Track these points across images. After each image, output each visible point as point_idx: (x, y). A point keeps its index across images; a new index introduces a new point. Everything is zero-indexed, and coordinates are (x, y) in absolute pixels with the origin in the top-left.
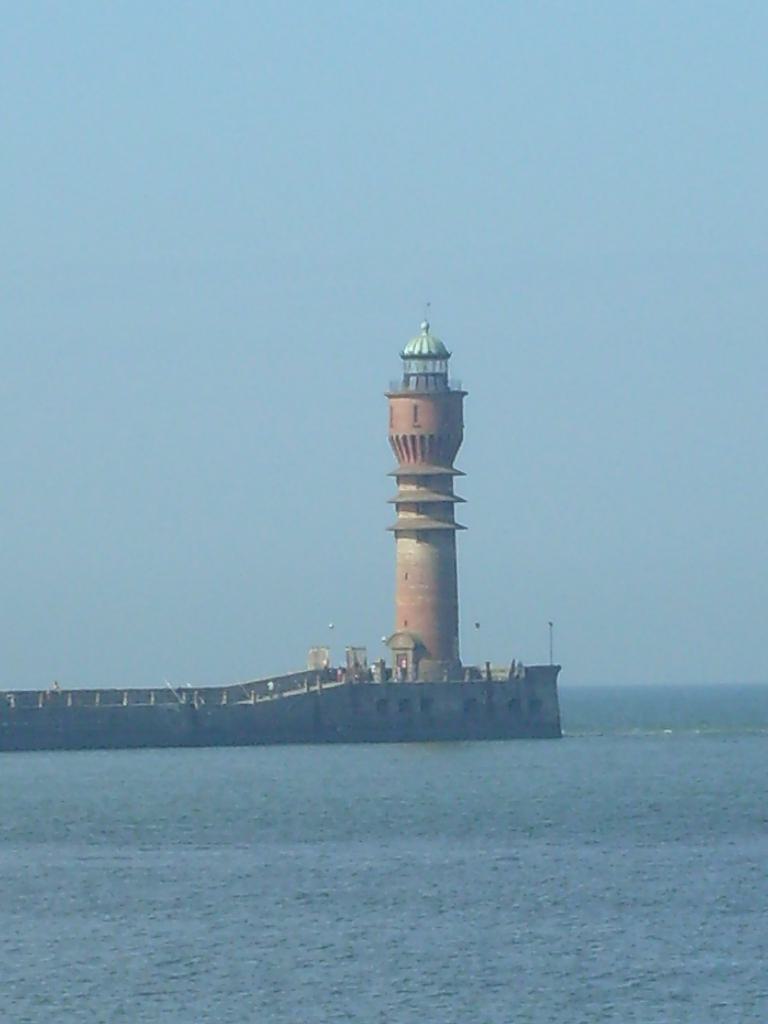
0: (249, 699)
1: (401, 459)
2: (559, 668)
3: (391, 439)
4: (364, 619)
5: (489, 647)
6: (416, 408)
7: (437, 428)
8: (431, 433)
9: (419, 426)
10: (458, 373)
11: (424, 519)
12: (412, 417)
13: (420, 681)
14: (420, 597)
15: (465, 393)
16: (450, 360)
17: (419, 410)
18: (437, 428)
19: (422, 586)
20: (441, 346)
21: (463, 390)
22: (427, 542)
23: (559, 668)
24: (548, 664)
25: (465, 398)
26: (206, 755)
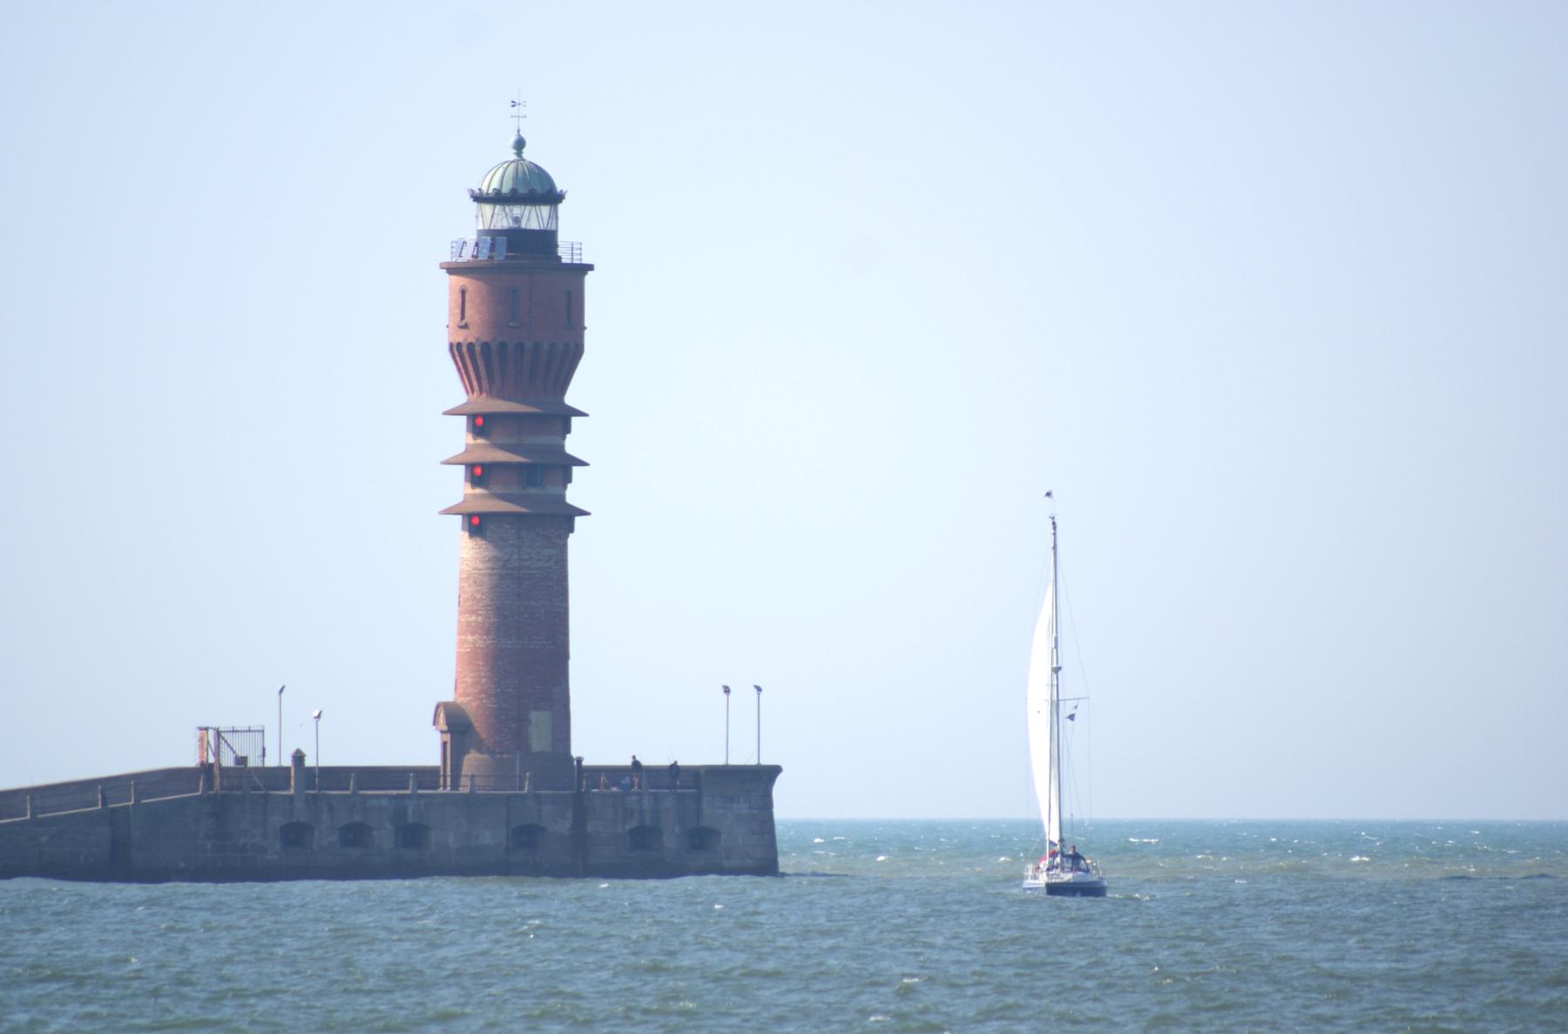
0: (436, 788)
1: (470, 389)
2: (775, 771)
3: (451, 346)
4: (380, 688)
5: (617, 718)
6: (463, 292)
7: (523, 317)
8: (485, 339)
9: (466, 327)
10: (576, 231)
11: (481, 496)
12: (458, 311)
13: (464, 790)
14: (470, 638)
15: (590, 267)
16: (560, 206)
17: (467, 297)
18: (523, 317)
19: (473, 618)
20: (540, 175)
21: (585, 261)
22: (484, 537)
23: (775, 771)
24: (753, 762)
25: (589, 278)
26: (559, 900)
